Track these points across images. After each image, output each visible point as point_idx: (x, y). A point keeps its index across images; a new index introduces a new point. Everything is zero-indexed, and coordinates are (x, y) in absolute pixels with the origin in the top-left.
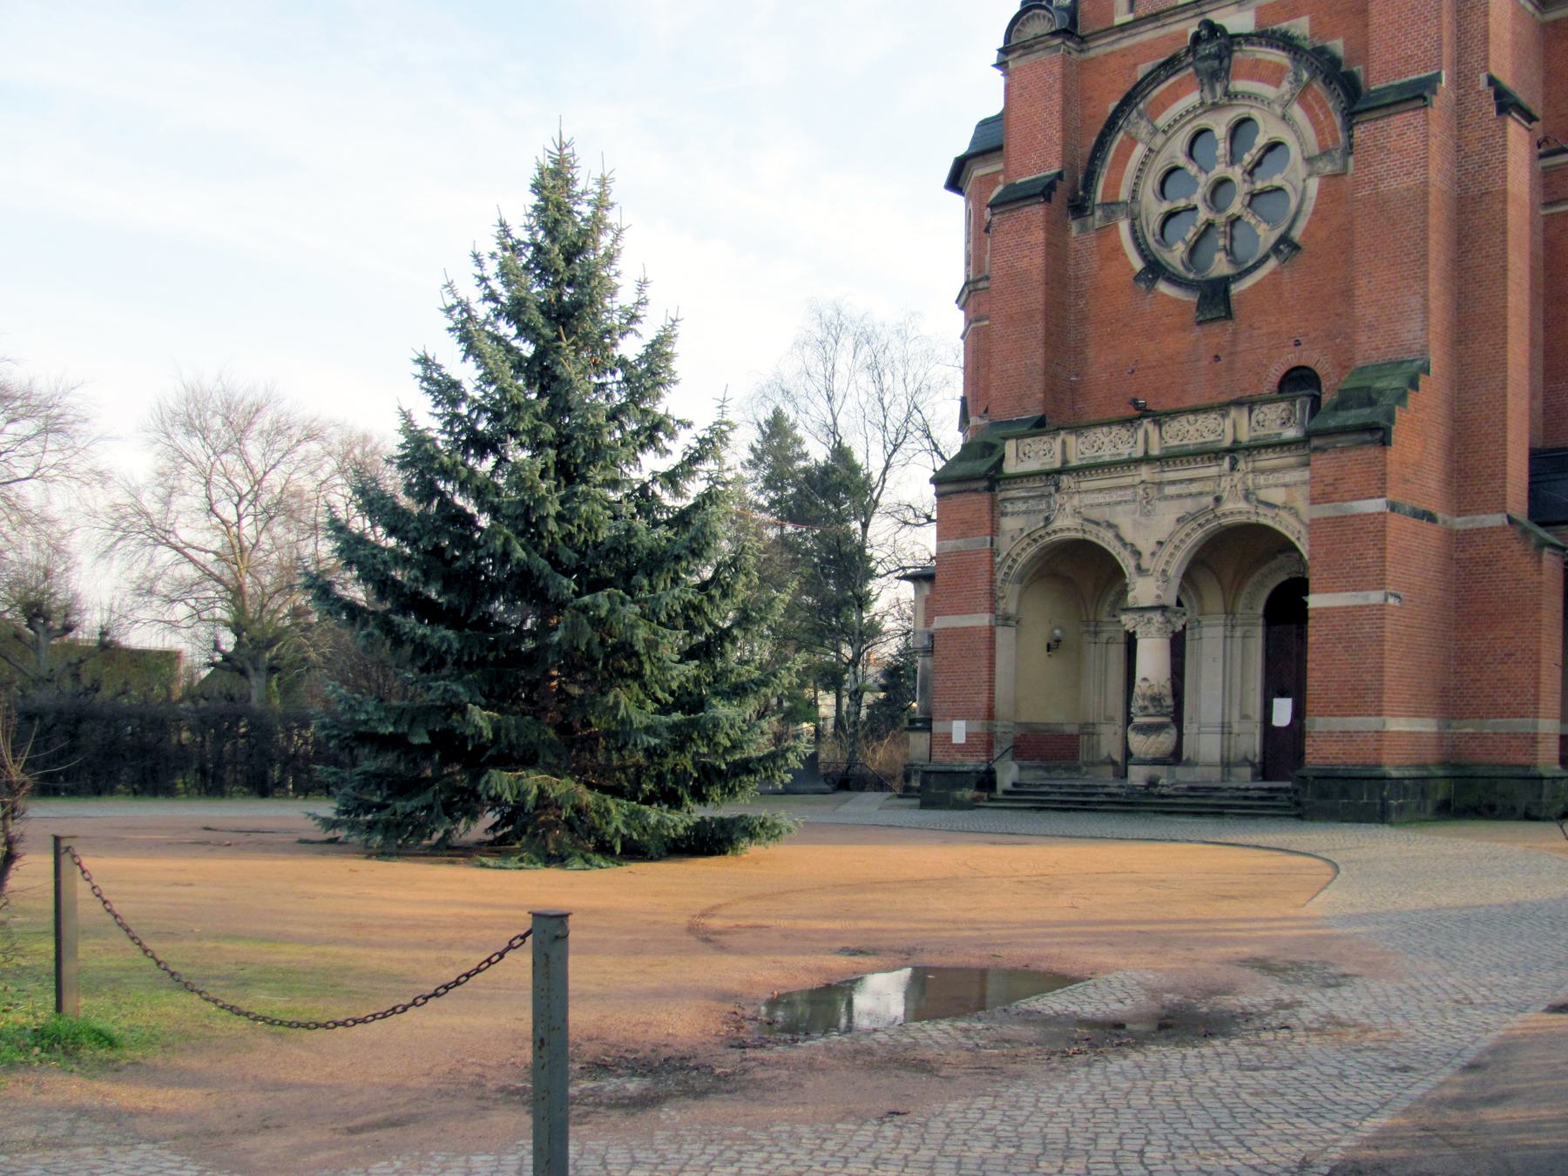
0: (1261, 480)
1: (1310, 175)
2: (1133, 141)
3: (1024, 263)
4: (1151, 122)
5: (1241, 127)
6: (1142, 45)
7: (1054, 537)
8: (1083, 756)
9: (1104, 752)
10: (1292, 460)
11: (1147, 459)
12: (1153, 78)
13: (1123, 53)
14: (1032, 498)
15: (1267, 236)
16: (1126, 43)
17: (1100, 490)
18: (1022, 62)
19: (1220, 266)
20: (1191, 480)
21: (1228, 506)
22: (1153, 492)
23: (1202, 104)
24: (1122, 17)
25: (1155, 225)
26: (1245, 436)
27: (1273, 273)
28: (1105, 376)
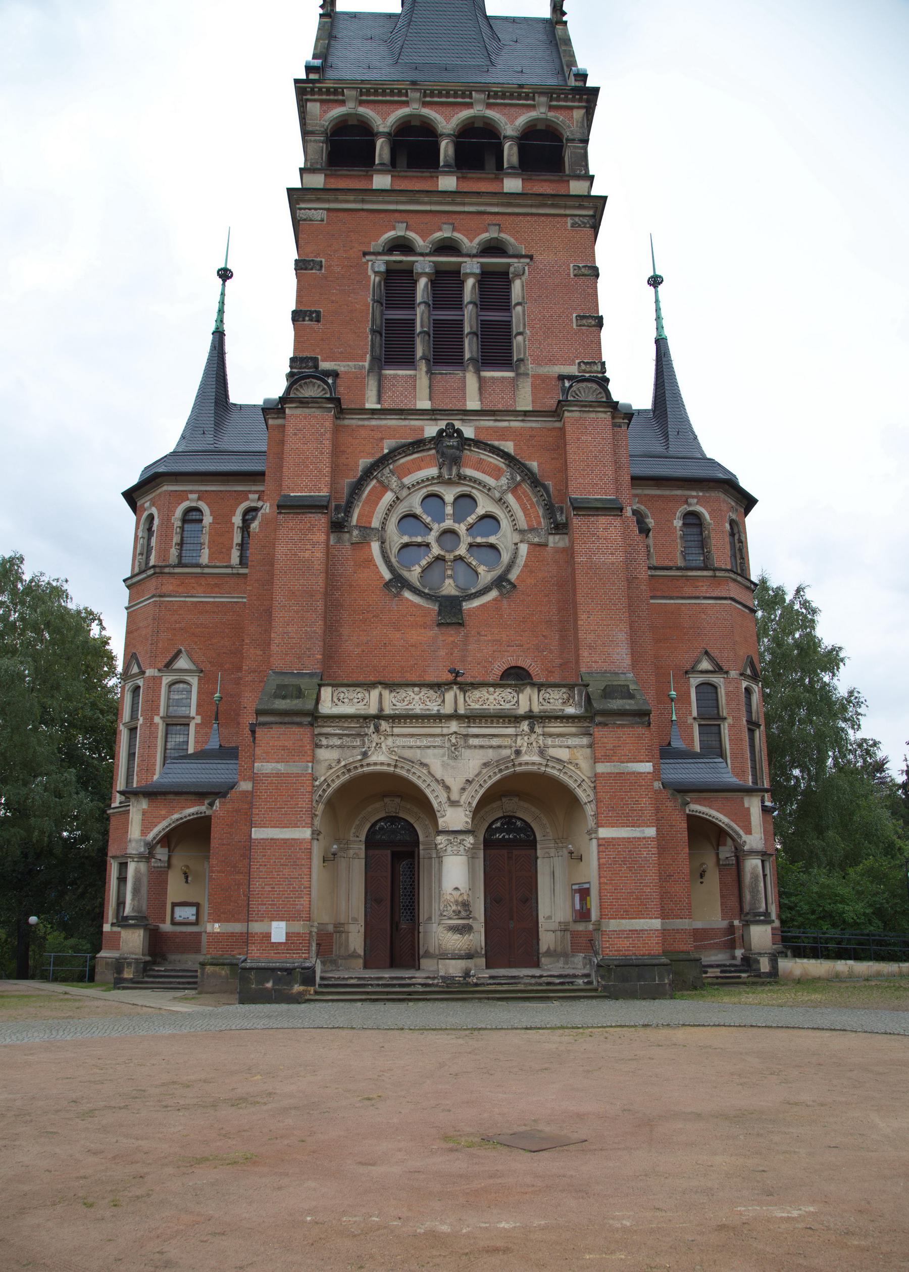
0: (549, 741)
1: (521, 542)
2: (385, 488)
3: (307, 554)
4: (400, 478)
6: (389, 427)
9: (352, 948)
10: (573, 730)
11: (455, 716)
12: (395, 453)
13: (373, 429)
15: (486, 575)
16: (374, 423)
17: (412, 735)
18: (298, 412)
19: (449, 588)
22: (461, 742)
23: (439, 477)
24: (371, 404)
25: (395, 550)
26: (536, 709)
27: (495, 600)
28: (358, 651)
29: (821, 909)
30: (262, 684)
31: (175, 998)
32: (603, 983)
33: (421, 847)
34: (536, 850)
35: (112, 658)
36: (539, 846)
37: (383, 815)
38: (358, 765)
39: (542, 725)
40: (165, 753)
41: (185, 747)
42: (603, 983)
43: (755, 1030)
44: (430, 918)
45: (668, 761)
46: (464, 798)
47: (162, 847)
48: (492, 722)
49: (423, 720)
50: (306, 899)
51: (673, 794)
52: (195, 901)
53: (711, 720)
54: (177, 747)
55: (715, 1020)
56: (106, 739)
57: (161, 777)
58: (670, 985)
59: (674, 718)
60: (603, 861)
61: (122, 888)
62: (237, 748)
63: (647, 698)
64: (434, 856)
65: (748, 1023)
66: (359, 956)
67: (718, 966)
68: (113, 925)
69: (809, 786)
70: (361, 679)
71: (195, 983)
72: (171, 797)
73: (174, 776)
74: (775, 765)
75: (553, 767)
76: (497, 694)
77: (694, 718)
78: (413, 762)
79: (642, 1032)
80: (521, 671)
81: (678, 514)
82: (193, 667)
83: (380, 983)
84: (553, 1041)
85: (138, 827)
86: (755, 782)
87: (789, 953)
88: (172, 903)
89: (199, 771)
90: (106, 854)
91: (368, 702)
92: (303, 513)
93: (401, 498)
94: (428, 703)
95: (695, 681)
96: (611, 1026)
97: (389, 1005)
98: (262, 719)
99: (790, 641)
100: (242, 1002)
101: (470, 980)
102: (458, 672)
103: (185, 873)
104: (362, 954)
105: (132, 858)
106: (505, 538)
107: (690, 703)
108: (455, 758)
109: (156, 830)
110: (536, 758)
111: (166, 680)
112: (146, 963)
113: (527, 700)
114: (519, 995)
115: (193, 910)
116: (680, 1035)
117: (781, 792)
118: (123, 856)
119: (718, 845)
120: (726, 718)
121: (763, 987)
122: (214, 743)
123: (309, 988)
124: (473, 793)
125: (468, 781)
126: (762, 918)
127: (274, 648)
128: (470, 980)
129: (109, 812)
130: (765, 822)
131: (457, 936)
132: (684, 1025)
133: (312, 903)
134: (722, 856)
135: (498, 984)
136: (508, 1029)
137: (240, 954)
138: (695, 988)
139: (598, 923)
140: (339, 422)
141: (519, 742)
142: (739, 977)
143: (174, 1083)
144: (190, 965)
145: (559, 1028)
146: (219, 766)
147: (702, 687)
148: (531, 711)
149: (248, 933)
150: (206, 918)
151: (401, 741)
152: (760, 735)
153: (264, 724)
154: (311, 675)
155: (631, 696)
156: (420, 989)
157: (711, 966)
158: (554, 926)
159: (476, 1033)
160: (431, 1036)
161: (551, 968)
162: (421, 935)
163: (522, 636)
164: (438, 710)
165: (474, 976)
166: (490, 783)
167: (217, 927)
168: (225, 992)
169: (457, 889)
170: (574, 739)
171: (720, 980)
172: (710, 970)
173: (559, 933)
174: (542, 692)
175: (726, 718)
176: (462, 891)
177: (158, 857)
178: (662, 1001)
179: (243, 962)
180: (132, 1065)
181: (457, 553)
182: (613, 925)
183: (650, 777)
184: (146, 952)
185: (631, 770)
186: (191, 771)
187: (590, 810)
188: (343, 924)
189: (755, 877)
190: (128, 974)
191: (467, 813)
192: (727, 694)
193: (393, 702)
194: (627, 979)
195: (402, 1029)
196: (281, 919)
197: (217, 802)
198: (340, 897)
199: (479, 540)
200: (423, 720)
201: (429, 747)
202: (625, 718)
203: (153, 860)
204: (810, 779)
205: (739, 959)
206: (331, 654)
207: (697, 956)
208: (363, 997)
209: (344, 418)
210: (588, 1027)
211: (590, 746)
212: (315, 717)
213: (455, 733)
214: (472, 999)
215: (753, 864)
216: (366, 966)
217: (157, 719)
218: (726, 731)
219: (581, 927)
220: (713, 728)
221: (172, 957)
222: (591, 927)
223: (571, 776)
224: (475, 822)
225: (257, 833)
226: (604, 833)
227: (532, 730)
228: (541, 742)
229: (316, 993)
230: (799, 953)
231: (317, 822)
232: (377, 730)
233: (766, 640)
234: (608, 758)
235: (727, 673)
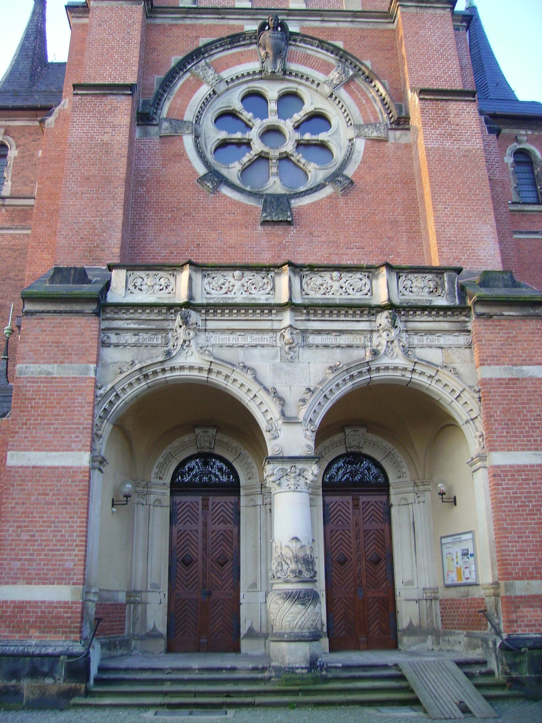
0: (415, 340)
1: (358, 136)
2: (199, 83)
3: (106, 138)
5: (290, 97)
7: (168, 375)
8: (128, 630)
10: (446, 326)
13: (187, 27)
16: (188, 22)
17: (233, 331)
19: (275, 185)
20: (341, 332)
22: (299, 339)
23: (261, 72)
27: (330, 197)
36: (392, 491)
37: (193, 451)
46: (302, 414)
48: (338, 314)
64: (260, 502)
66: (160, 636)
75: (422, 373)
78: (234, 365)
81: (508, 151)
92: (104, 95)
93: (218, 92)
94: (253, 291)
106: (339, 136)
110: (400, 361)
125: (309, 390)
140: (150, 21)
151: (216, 339)
158: (415, 594)
163: (363, 237)
166: (337, 394)
169: (296, 539)
174: (402, 278)
176: (304, 542)
181: (283, 150)
188: (140, 592)
191: (309, 433)
199: (307, 136)
209: (155, 18)
212: (100, 304)
216: (169, 649)
224: (320, 447)
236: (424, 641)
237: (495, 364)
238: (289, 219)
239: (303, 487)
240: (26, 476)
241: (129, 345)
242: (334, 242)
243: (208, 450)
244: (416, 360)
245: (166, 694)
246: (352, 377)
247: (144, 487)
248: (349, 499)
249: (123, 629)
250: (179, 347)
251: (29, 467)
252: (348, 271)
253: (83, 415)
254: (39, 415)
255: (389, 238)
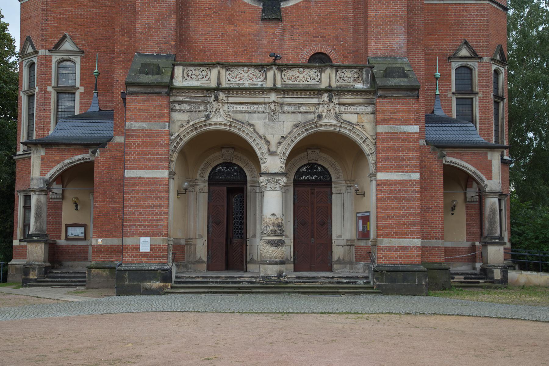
0: (343, 109)
7: (208, 128)
9: (198, 256)
10: (361, 101)
11: (274, 89)
14: (195, 103)
17: (243, 103)
21: (325, 121)
22: (278, 109)
26: (334, 85)
28: (202, 39)
29: (543, 236)
30: (129, 63)
31: (69, 292)
32: (378, 283)
33: (248, 185)
34: (331, 188)
35: (11, 41)
36: (333, 185)
37: (221, 161)
38: (203, 124)
39: (338, 97)
40: (57, 114)
41: (73, 110)
42: (378, 283)
43: (488, 319)
44: (254, 236)
45: (431, 125)
46: (280, 150)
47: (57, 184)
48: (301, 94)
49: (250, 92)
50: (165, 221)
51: (433, 149)
52: (83, 223)
53: (466, 94)
54: (66, 110)
55: (458, 311)
56: (10, 103)
57: (55, 132)
58: (426, 285)
59: (438, 93)
60: (379, 196)
61: (27, 214)
62: (112, 111)
63: (417, 77)
64: (258, 191)
65: (483, 314)
66: (203, 262)
67: (462, 274)
68: (20, 240)
69: (540, 145)
70: (205, 60)
71: (84, 281)
72: (63, 147)
73: (65, 131)
74: (514, 129)
76: (305, 73)
77: (453, 93)
79: (404, 318)
80: (323, 56)
82: (76, 49)
83: (218, 280)
84: (340, 322)
85: (37, 170)
86: (497, 141)
87: (517, 267)
88: (66, 225)
89: (84, 128)
90: (14, 190)
91: (211, 78)
94: (254, 79)
95: (455, 64)
96: (382, 313)
97: (225, 296)
98: (131, 89)
99: (534, 33)
100: (118, 294)
101: (282, 279)
102: (277, 56)
103: (75, 203)
104: (206, 260)
105: (35, 191)
107: (450, 82)
108: (274, 120)
109: (52, 171)
110: (333, 121)
111: (55, 59)
112: (47, 268)
113: (327, 78)
114: (317, 290)
115: (82, 230)
116: (432, 320)
117: (517, 149)
118: (27, 191)
119: (466, 187)
120: (477, 93)
121: (496, 290)
122: (94, 108)
123: (167, 284)
124: (286, 146)
125: (283, 137)
126: (497, 241)
127: (138, 35)
128: (282, 279)
129: (15, 158)
130: (503, 171)
131: (273, 248)
132: (435, 314)
133: (169, 224)
134: (468, 195)
135: (303, 282)
136: (308, 313)
137: (117, 260)
138: (445, 289)
139: (375, 241)
141: (321, 109)
142: (478, 283)
143: (68, 350)
144: (80, 269)
145: (345, 313)
146: (99, 124)
147: (460, 69)
148: (330, 86)
149: (122, 245)
150: (91, 236)
151: (234, 108)
152: (503, 106)
153: (132, 93)
154: (167, 57)
155: (405, 76)
156: (247, 285)
157: (457, 274)
158: (343, 242)
159: (286, 315)
160: (254, 317)
161: (340, 272)
162: (248, 247)
163: (325, 29)
164: (262, 85)
165: (285, 276)
167: (100, 242)
168: (107, 287)
169: (274, 215)
170: (361, 107)
171: (463, 284)
172: (456, 277)
173: (347, 247)
174: (339, 72)
175: (477, 93)
177: (55, 191)
178: (420, 297)
179: (119, 266)
180: (36, 338)
182: (386, 242)
183: (417, 136)
184: (47, 259)
185: (402, 131)
186: (78, 128)
187: (371, 159)
189: (493, 211)
190: (33, 276)
191: (282, 160)
192: (480, 75)
193: (228, 78)
194: (394, 281)
195: (234, 312)
196: (147, 235)
197: (98, 151)
198: (191, 220)
200: (250, 92)
201: (254, 112)
202: (400, 92)
203: (51, 193)
204: (542, 139)
205: (478, 270)
206: (181, 41)
207: (447, 266)
208: (206, 290)
210: (366, 313)
211: (373, 113)
212: (170, 89)
213: (274, 102)
214: (284, 292)
215: (492, 202)
216: (208, 269)
217: (50, 89)
218: (477, 103)
219: (362, 243)
220: (467, 100)
221: (66, 263)
222: (370, 244)
223: (358, 135)
224: (288, 167)
225: (129, 174)
226: (381, 176)
227: (331, 101)
228: (337, 109)
229: (172, 287)
230: (524, 267)
231: (173, 166)
232: (216, 99)
233: (514, 33)
234: (386, 122)
235: (481, 58)
236: (345, 267)
237: (385, 125)
238: (279, 17)
239: (278, 188)
240: (135, 183)
241: (186, 110)
242: (306, 33)
243: (229, 161)
244: (342, 121)
245: (209, 288)
246: (307, 130)
247: (193, 183)
248: (309, 189)
249: (184, 258)
250: (213, 113)
251: (136, 178)
252: (308, 68)
253: (163, 152)
254: (140, 151)
255: (341, 29)
